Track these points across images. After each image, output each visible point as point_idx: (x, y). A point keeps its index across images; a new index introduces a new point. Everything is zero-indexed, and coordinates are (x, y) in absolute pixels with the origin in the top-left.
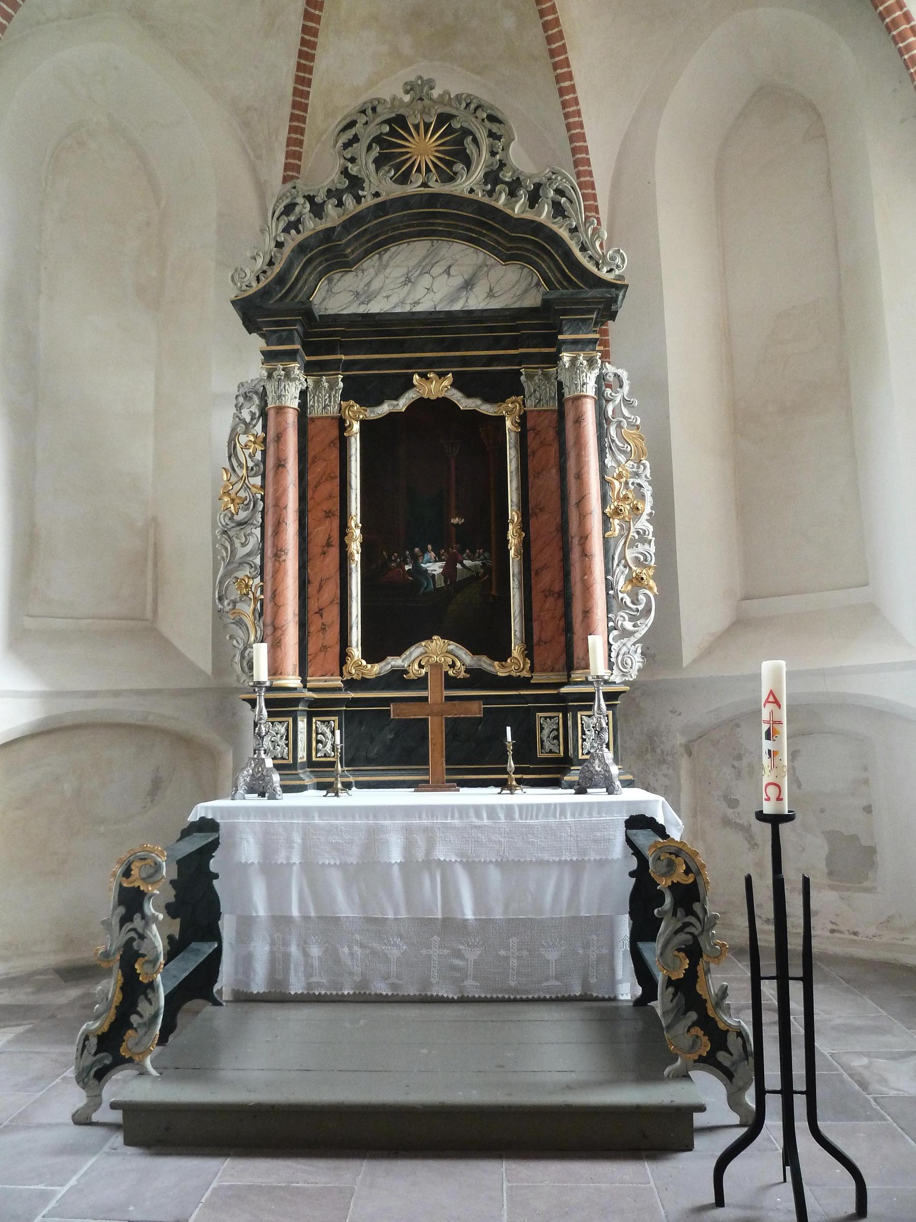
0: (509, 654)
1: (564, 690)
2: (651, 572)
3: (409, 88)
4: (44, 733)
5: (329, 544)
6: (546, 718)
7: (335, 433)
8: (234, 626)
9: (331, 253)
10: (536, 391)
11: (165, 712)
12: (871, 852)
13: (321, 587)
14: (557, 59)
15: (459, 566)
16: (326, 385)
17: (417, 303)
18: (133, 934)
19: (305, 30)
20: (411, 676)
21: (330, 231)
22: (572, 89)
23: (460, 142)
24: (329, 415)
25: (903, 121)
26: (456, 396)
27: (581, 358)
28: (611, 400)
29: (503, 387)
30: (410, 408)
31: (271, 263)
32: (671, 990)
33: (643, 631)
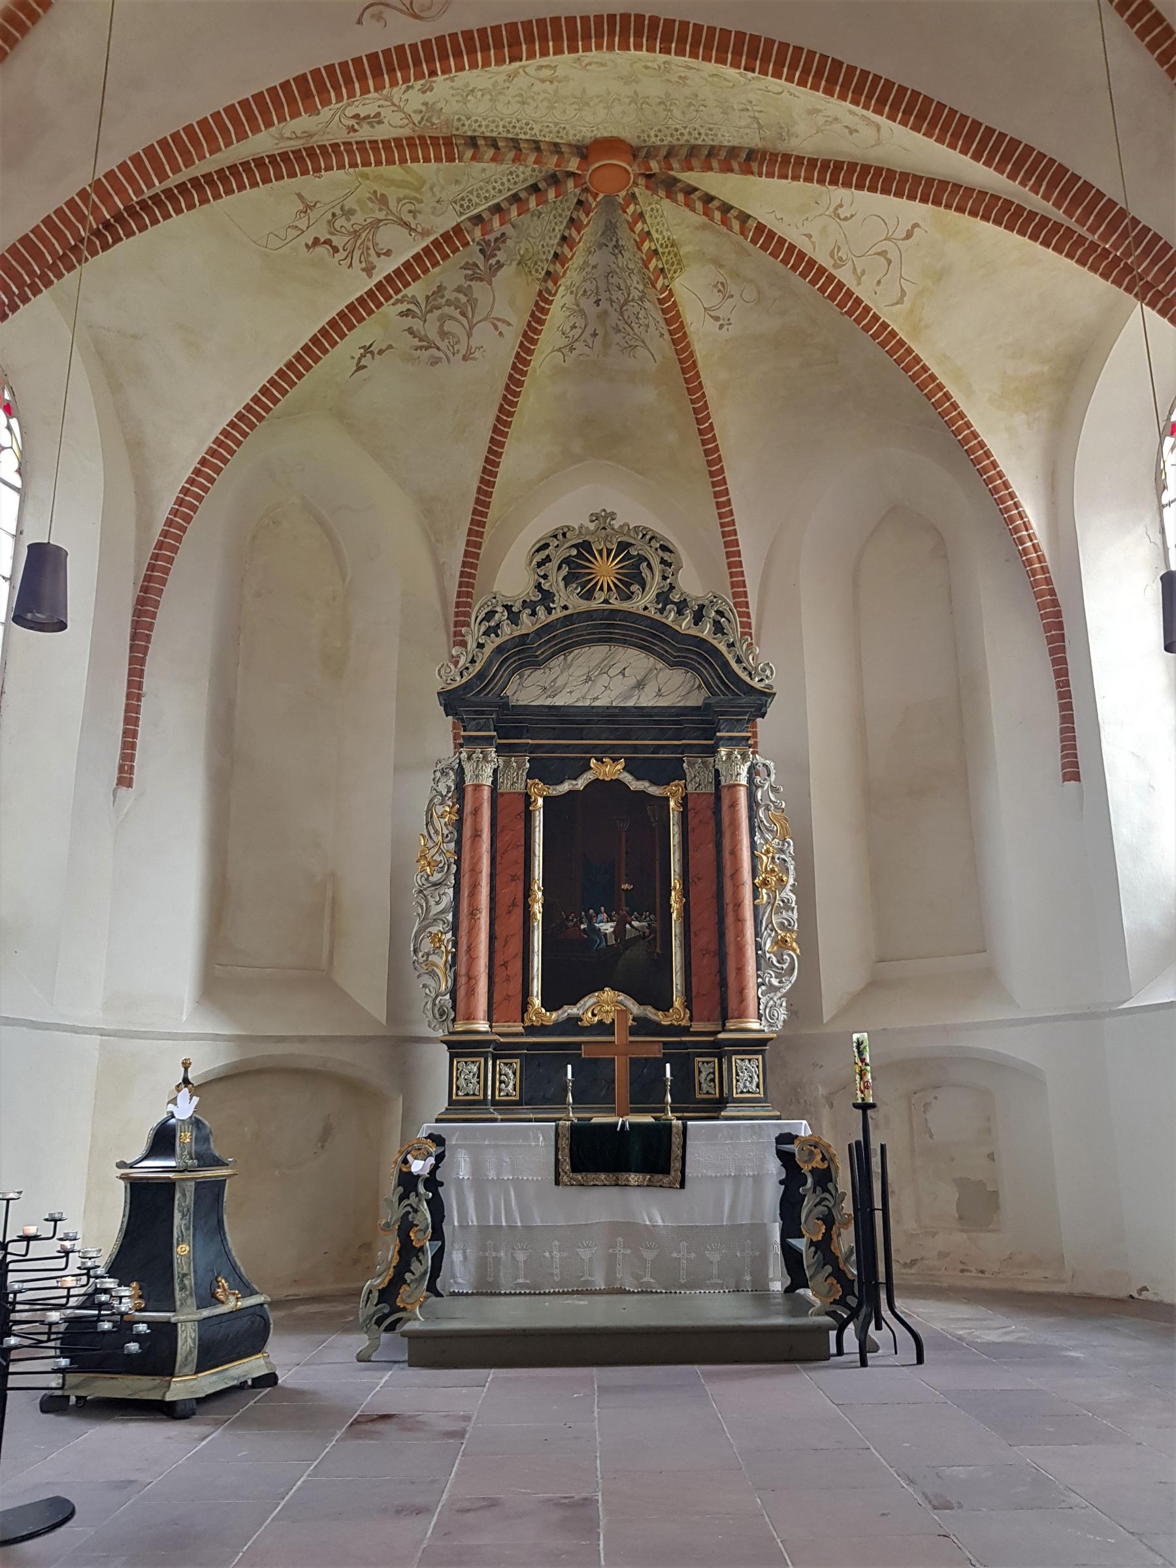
1: (721, 1036)
5: (514, 905)
7: (522, 807)
9: (524, 654)
12: (995, 1193)
13: (506, 942)
17: (596, 698)
19: (492, 440)
26: (627, 778)
29: (667, 772)
31: (473, 661)
32: (813, 1249)
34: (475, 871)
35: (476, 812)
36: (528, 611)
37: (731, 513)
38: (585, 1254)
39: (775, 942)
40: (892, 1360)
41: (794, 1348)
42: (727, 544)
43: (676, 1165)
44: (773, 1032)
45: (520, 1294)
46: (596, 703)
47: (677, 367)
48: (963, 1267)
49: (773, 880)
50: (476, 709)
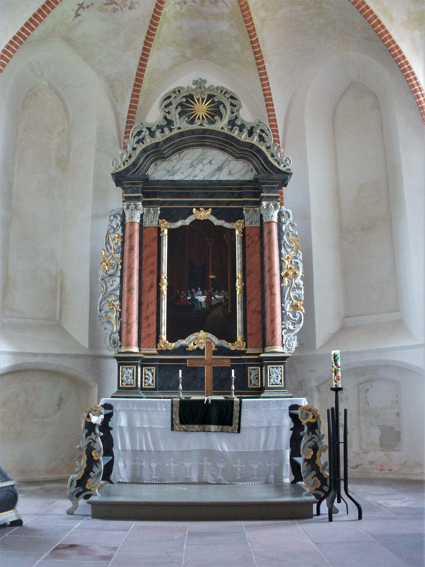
0: (236, 339)
1: (262, 355)
2: (302, 303)
3: (195, 83)
4: (14, 372)
5: (152, 286)
6: (252, 369)
7: (156, 234)
8: (106, 324)
9: (157, 153)
10: (250, 218)
11: (67, 365)
12: (399, 433)
13: (148, 306)
14: (260, 67)
15: (213, 298)
16: (152, 212)
17: (196, 176)
18: (91, 441)
19: (144, 49)
20: (190, 349)
21: (157, 145)
22: (267, 79)
23: (218, 107)
24: (153, 226)
25: (411, 108)
26: (213, 219)
27: (271, 204)
28: (285, 223)
29: (235, 215)
30: (191, 223)
31: (130, 157)
32: (306, 463)
33: (298, 330)
34: (131, 268)
35: (131, 236)
36: (160, 130)
37: (268, 84)
38: (187, 465)
39: (292, 306)
40: (346, 518)
41: (296, 513)
42: (266, 100)
43: (236, 421)
44: (289, 353)
45: (154, 483)
46: (196, 179)
47: (239, 9)
48: (382, 468)
49: (291, 273)
50: (131, 181)
